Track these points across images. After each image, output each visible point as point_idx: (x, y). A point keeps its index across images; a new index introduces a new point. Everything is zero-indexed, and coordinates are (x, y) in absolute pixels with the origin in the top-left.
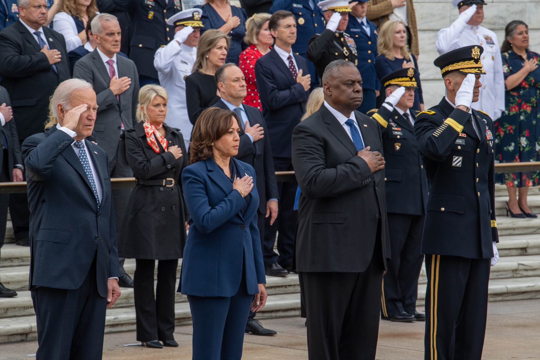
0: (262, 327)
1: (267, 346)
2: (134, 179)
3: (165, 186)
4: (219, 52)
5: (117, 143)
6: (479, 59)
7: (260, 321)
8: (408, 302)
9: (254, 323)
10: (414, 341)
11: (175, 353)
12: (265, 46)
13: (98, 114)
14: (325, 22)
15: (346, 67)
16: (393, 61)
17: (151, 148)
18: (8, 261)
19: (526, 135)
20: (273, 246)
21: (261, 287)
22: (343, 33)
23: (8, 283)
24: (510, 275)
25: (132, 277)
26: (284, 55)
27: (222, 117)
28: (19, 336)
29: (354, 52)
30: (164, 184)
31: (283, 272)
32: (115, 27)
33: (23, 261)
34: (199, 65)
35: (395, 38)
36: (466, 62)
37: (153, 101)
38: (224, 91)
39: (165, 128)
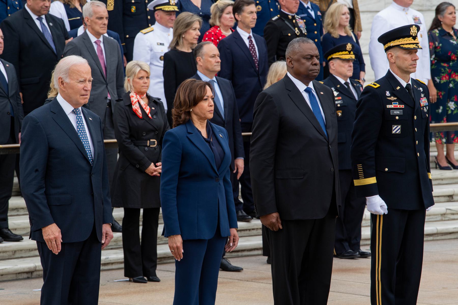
0: (230, 264)
1: (235, 281)
2: (115, 140)
3: (149, 146)
5: (104, 112)
9: (224, 261)
11: (157, 287)
13: (93, 85)
14: (279, 6)
15: (306, 44)
16: (339, 39)
17: (134, 113)
19: (455, 100)
20: (238, 196)
21: (233, 231)
22: (294, 16)
23: (16, 229)
24: (440, 218)
25: (121, 224)
26: (245, 35)
27: (197, 86)
28: (25, 274)
29: (304, 31)
30: (148, 145)
31: (248, 217)
32: (104, 12)
35: (342, 18)
36: (406, 39)
37: (138, 75)
38: (202, 65)
39: (148, 97)
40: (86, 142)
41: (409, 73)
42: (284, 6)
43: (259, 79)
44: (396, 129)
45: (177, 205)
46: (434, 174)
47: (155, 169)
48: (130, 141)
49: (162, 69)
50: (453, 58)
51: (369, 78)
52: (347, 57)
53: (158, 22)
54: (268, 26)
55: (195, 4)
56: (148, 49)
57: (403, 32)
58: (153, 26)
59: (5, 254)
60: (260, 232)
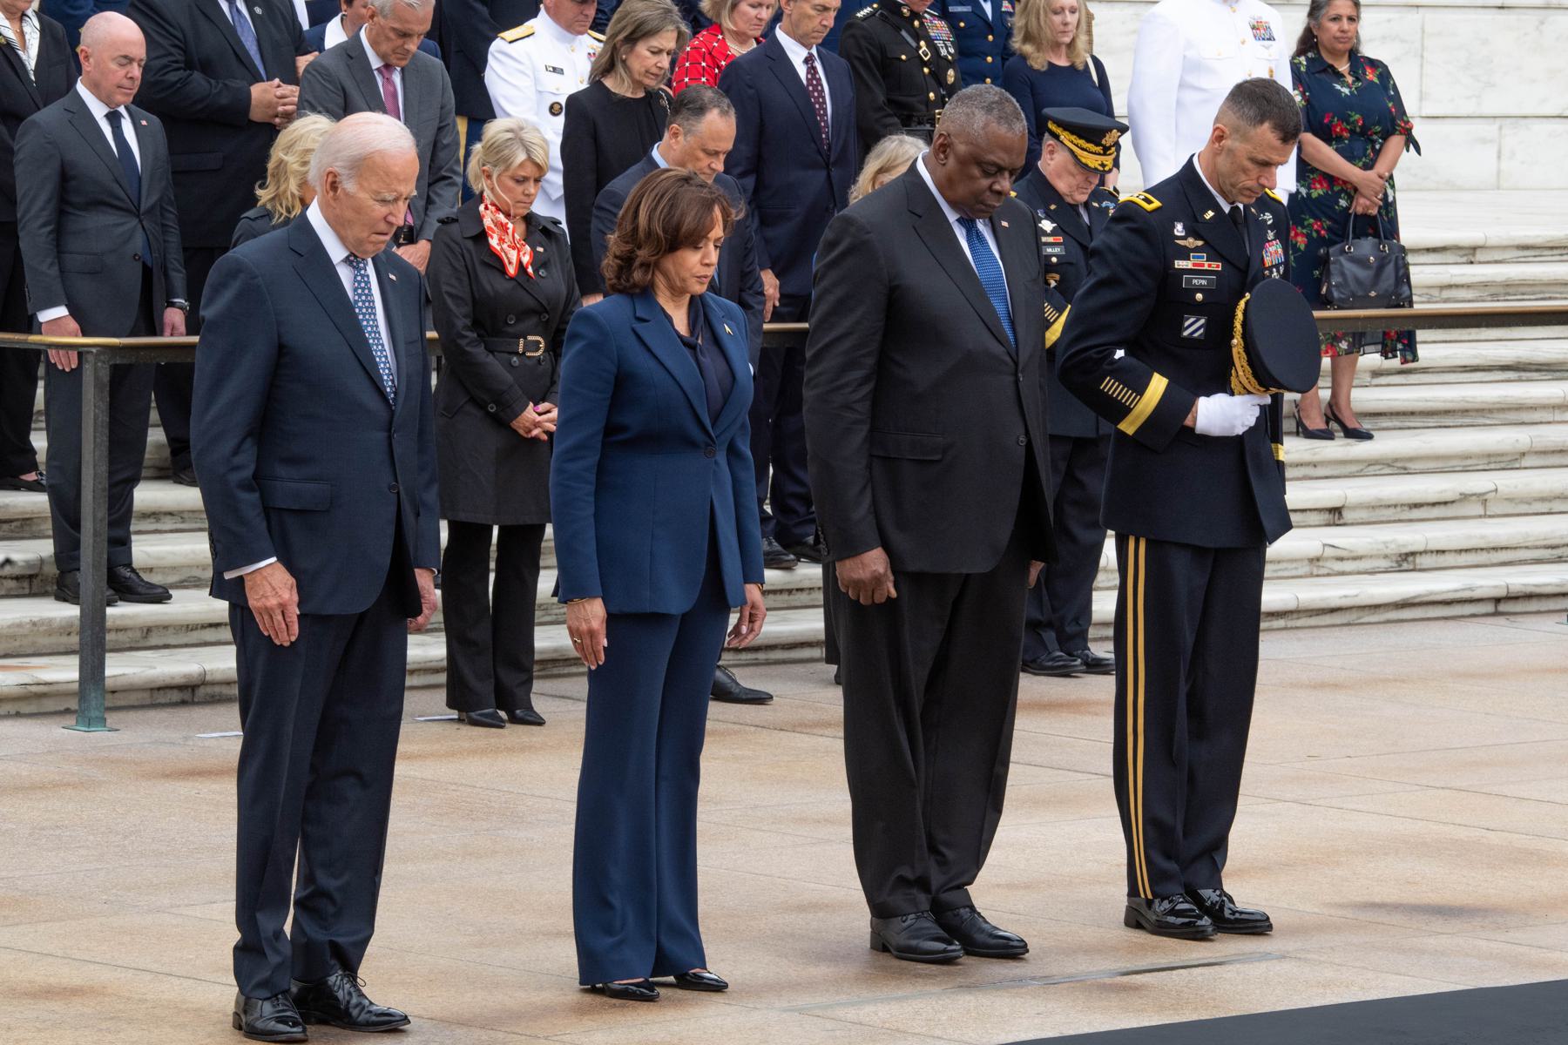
7: (734, 670)
8: (1070, 629)
10: (1088, 719)
21: (753, 591)
23: (151, 570)
24: (1305, 569)
26: (797, 54)
28: (175, 692)
33: (183, 520)
43: (829, 176)
44: (1194, 327)
45: (595, 515)
47: (540, 418)
60: (819, 597)
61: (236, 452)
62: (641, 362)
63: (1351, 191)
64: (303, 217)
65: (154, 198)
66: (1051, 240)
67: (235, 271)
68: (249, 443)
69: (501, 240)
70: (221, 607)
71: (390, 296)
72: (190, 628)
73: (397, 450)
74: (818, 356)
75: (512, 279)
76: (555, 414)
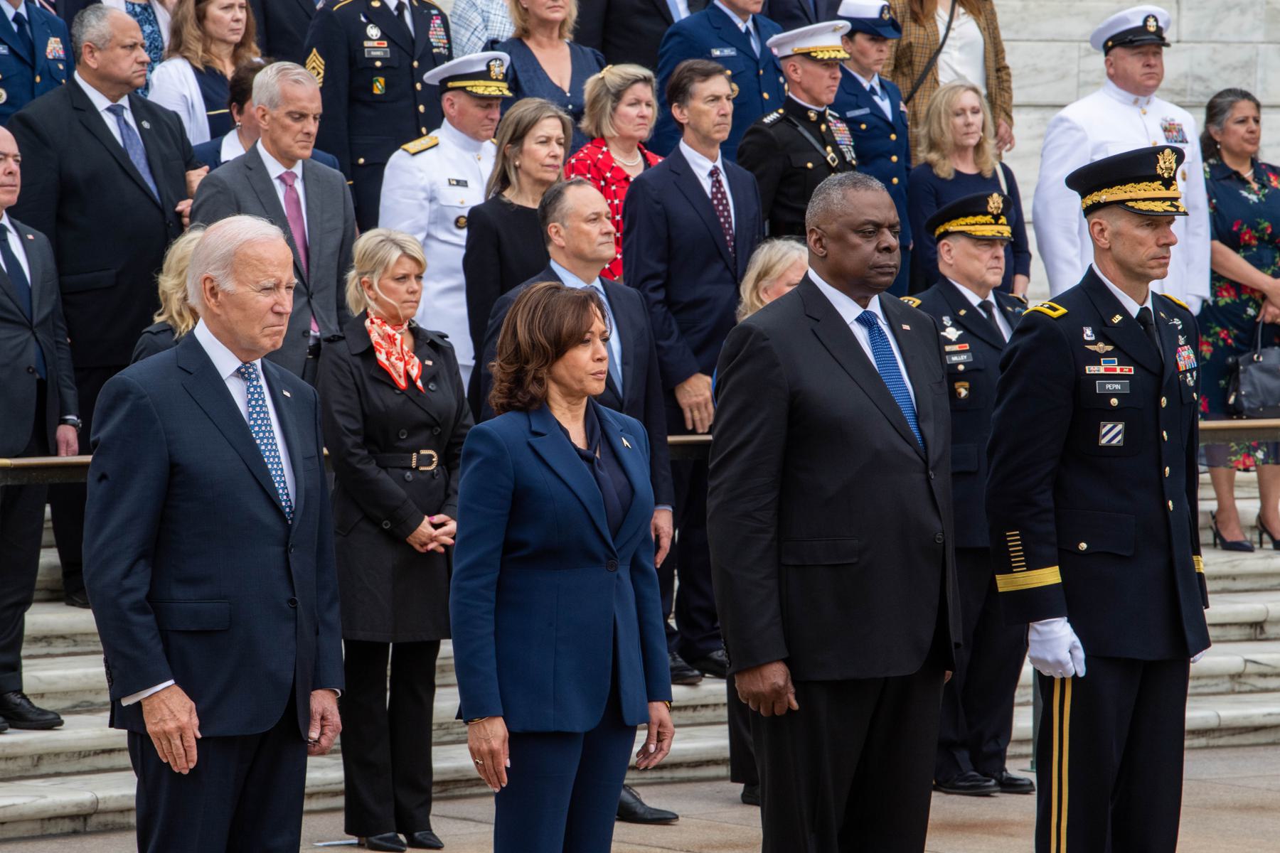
0: (642, 804)
3: (417, 468)
4: (543, 151)
6: (1174, 178)
10: (1002, 840)
12: (628, 144)
18: (40, 644)
21: (659, 710)
23: (42, 695)
24: (1226, 686)
28: (67, 822)
29: (850, 156)
30: (414, 465)
31: (691, 674)
32: (311, 100)
33: (76, 643)
34: (502, 179)
36: (1143, 185)
39: (415, 332)
40: (274, 457)
41: (1147, 278)
42: (799, 83)
44: (1111, 434)
45: (496, 634)
46: (1210, 562)
47: (437, 531)
48: (366, 452)
49: (463, 251)
50: (1247, 237)
51: (1037, 292)
52: (989, 231)
53: (452, 122)
54: (748, 139)
55: (556, 81)
56: (423, 195)
57: (1137, 166)
58: (435, 133)
59: (11, 765)
60: (724, 713)
61: (127, 574)
62: (538, 474)
63: (1260, 298)
64: (191, 334)
65: (46, 310)
66: (956, 348)
67: (123, 394)
68: (141, 565)
69: (389, 354)
70: (120, 737)
71: (286, 412)
72: (83, 754)
73: (295, 566)
74: (720, 466)
75: (403, 392)
76: (452, 526)
